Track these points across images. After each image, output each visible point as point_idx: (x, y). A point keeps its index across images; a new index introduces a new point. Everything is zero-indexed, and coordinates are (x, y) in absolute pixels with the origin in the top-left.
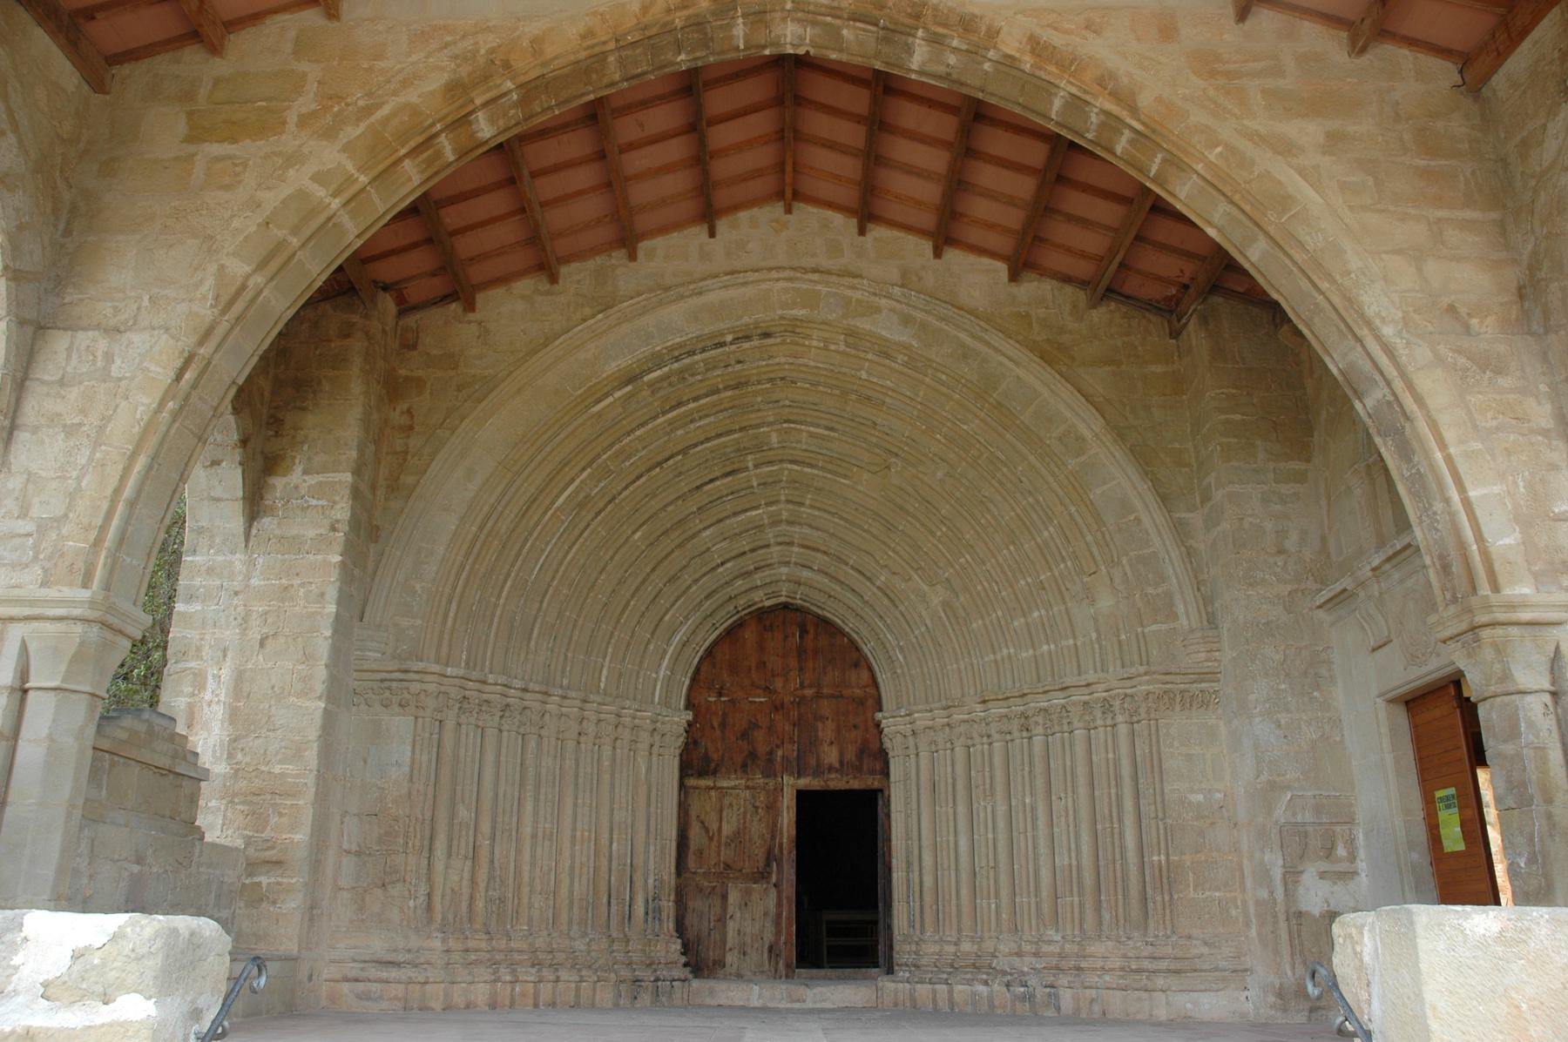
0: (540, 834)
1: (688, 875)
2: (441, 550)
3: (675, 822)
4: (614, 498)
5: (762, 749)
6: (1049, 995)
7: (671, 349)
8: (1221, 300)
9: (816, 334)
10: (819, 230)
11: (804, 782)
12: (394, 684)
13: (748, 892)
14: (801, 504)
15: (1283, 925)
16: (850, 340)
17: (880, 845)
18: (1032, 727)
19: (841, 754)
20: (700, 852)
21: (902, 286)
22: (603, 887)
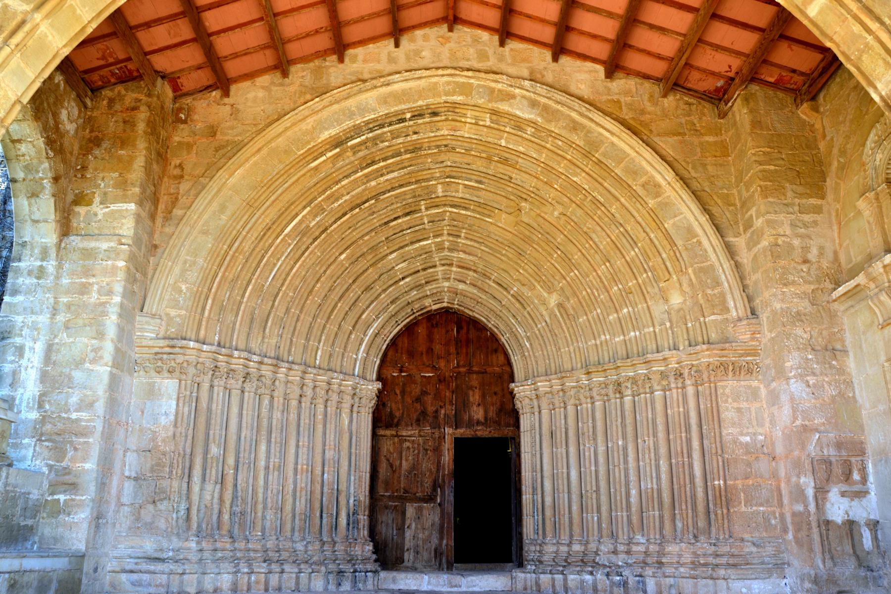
0: (271, 467)
3: (369, 459)
4: (326, 229)
5: (431, 409)
6: (639, 582)
7: (367, 123)
8: (758, 88)
9: (469, 113)
10: (473, 44)
11: (461, 432)
12: (165, 356)
13: (420, 509)
14: (459, 236)
15: (815, 530)
16: (494, 117)
17: (513, 476)
18: (623, 389)
21: (531, 80)
22: (317, 505)
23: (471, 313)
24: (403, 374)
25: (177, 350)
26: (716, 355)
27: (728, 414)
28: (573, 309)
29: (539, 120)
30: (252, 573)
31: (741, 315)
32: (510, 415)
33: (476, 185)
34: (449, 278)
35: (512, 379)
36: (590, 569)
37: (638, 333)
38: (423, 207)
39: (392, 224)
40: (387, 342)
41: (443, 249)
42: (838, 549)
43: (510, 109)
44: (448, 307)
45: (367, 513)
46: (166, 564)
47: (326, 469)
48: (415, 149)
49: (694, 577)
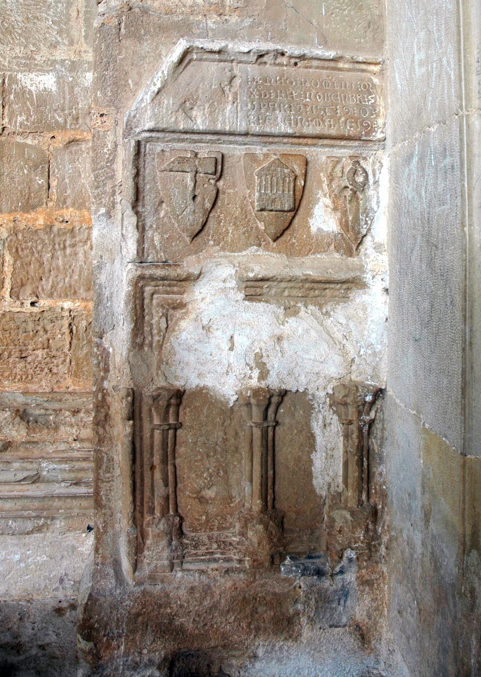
42: (210, 493)
49: (102, 406)
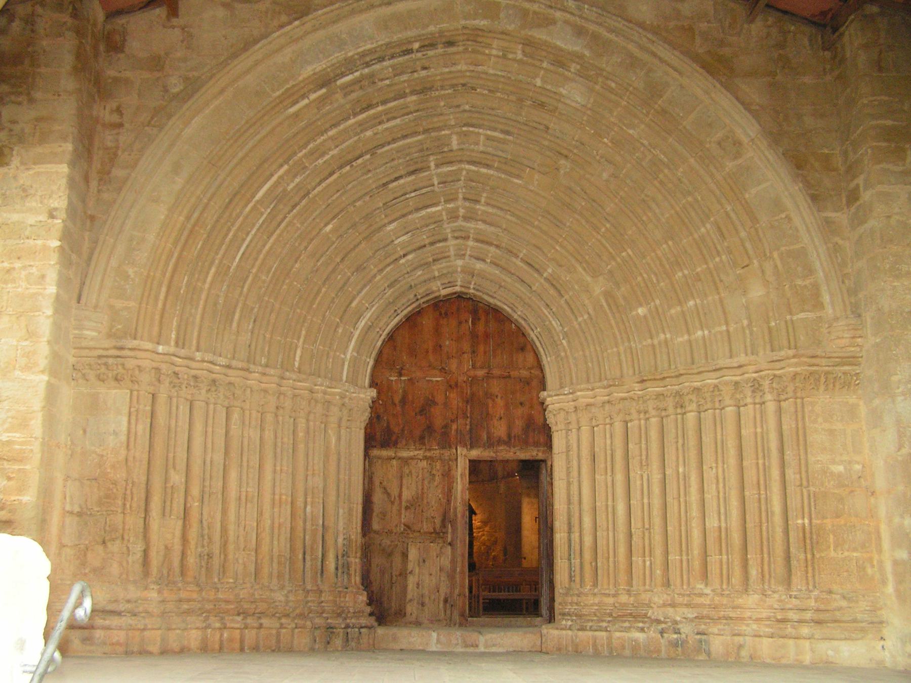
1: (372, 535)
2: (151, 237)
3: (361, 487)
4: (308, 193)
5: (438, 422)
6: (700, 641)
7: (363, 55)
11: (475, 453)
12: (110, 361)
14: (477, 201)
16: (528, 49)
19: (510, 428)
20: (384, 514)
22: (299, 545)
23: (492, 301)
24: (403, 378)
25: (126, 353)
26: (805, 363)
27: (817, 438)
28: (625, 298)
29: (587, 53)
30: (225, 628)
31: (838, 315)
32: (542, 433)
33: (501, 136)
34: (464, 255)
35: (543, 386)
36: (641, 625)
37: (706, 332)
38: (432, 165)
39: (391, 186)
40: (383, 337)
41: (457, 217)
43: (549, 39)
44: (461, 292)
45: (359, 555)
46: (124, 618)
47: (309, 500)
48: (424, 89)
